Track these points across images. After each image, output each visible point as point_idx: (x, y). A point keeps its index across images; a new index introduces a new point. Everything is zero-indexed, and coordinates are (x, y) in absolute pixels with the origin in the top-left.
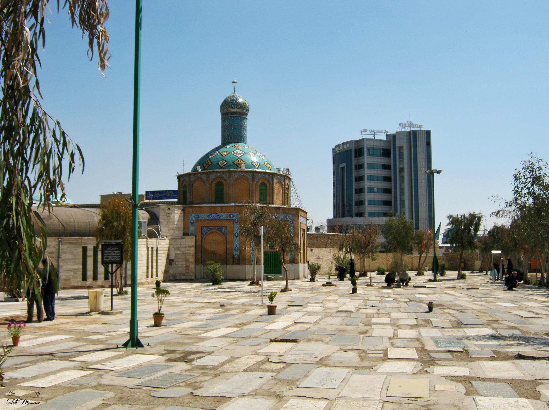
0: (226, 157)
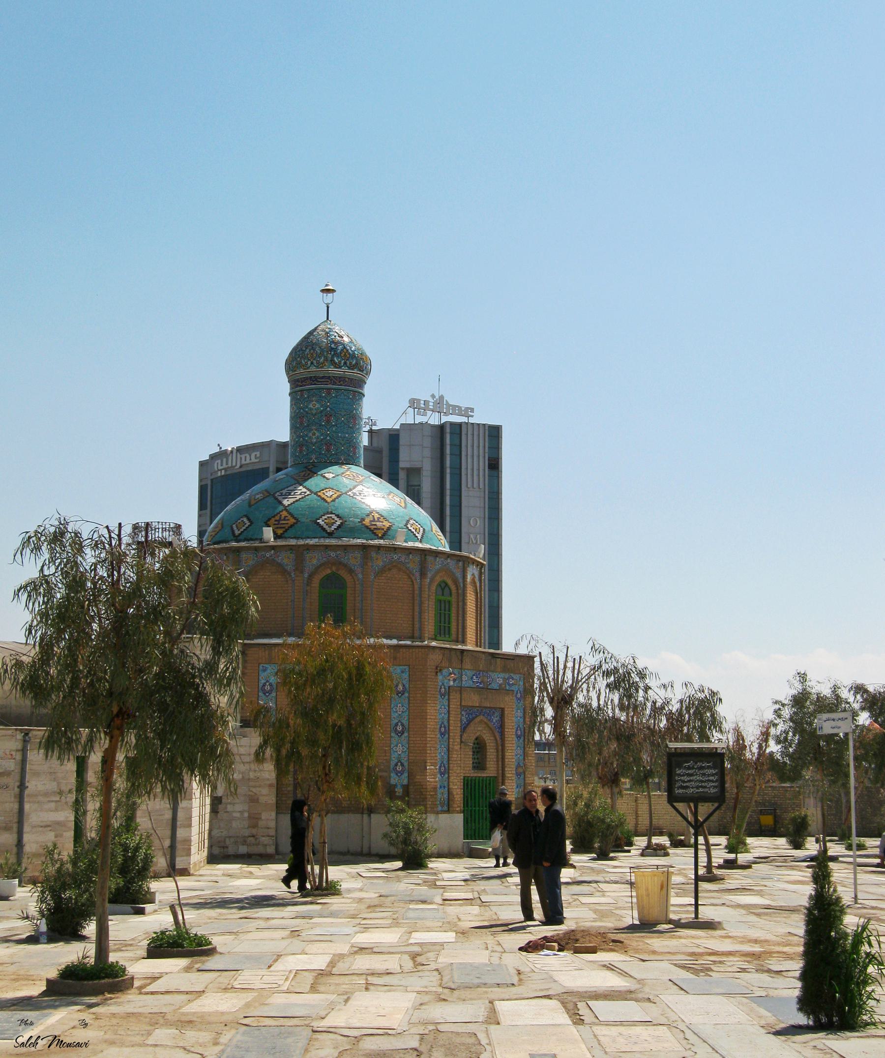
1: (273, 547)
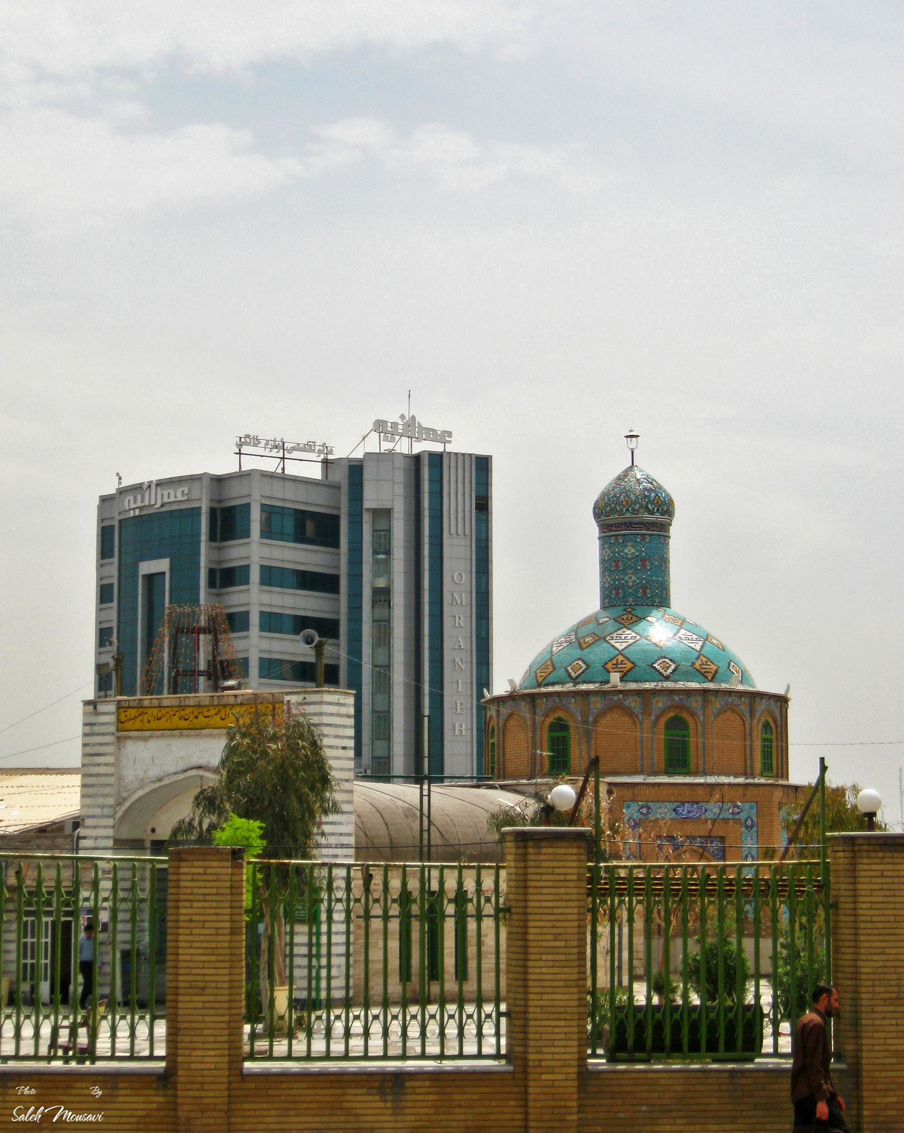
1: (621, 692)
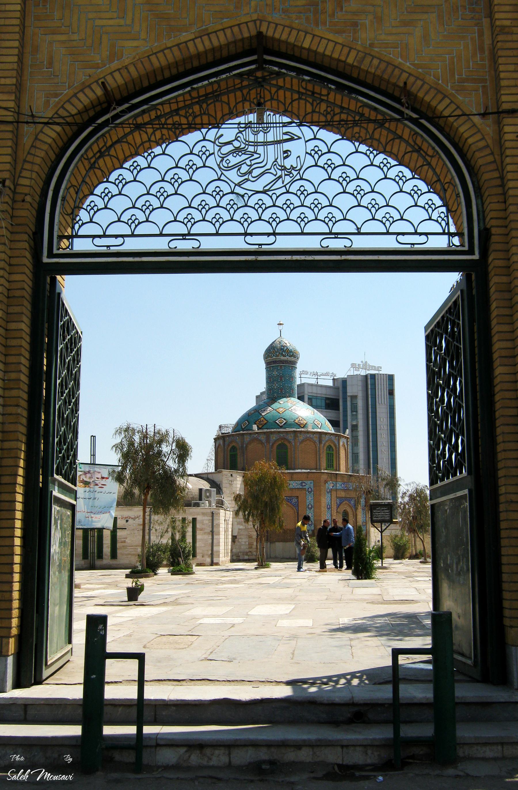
0: (284, 414)
1: (257, 433)
